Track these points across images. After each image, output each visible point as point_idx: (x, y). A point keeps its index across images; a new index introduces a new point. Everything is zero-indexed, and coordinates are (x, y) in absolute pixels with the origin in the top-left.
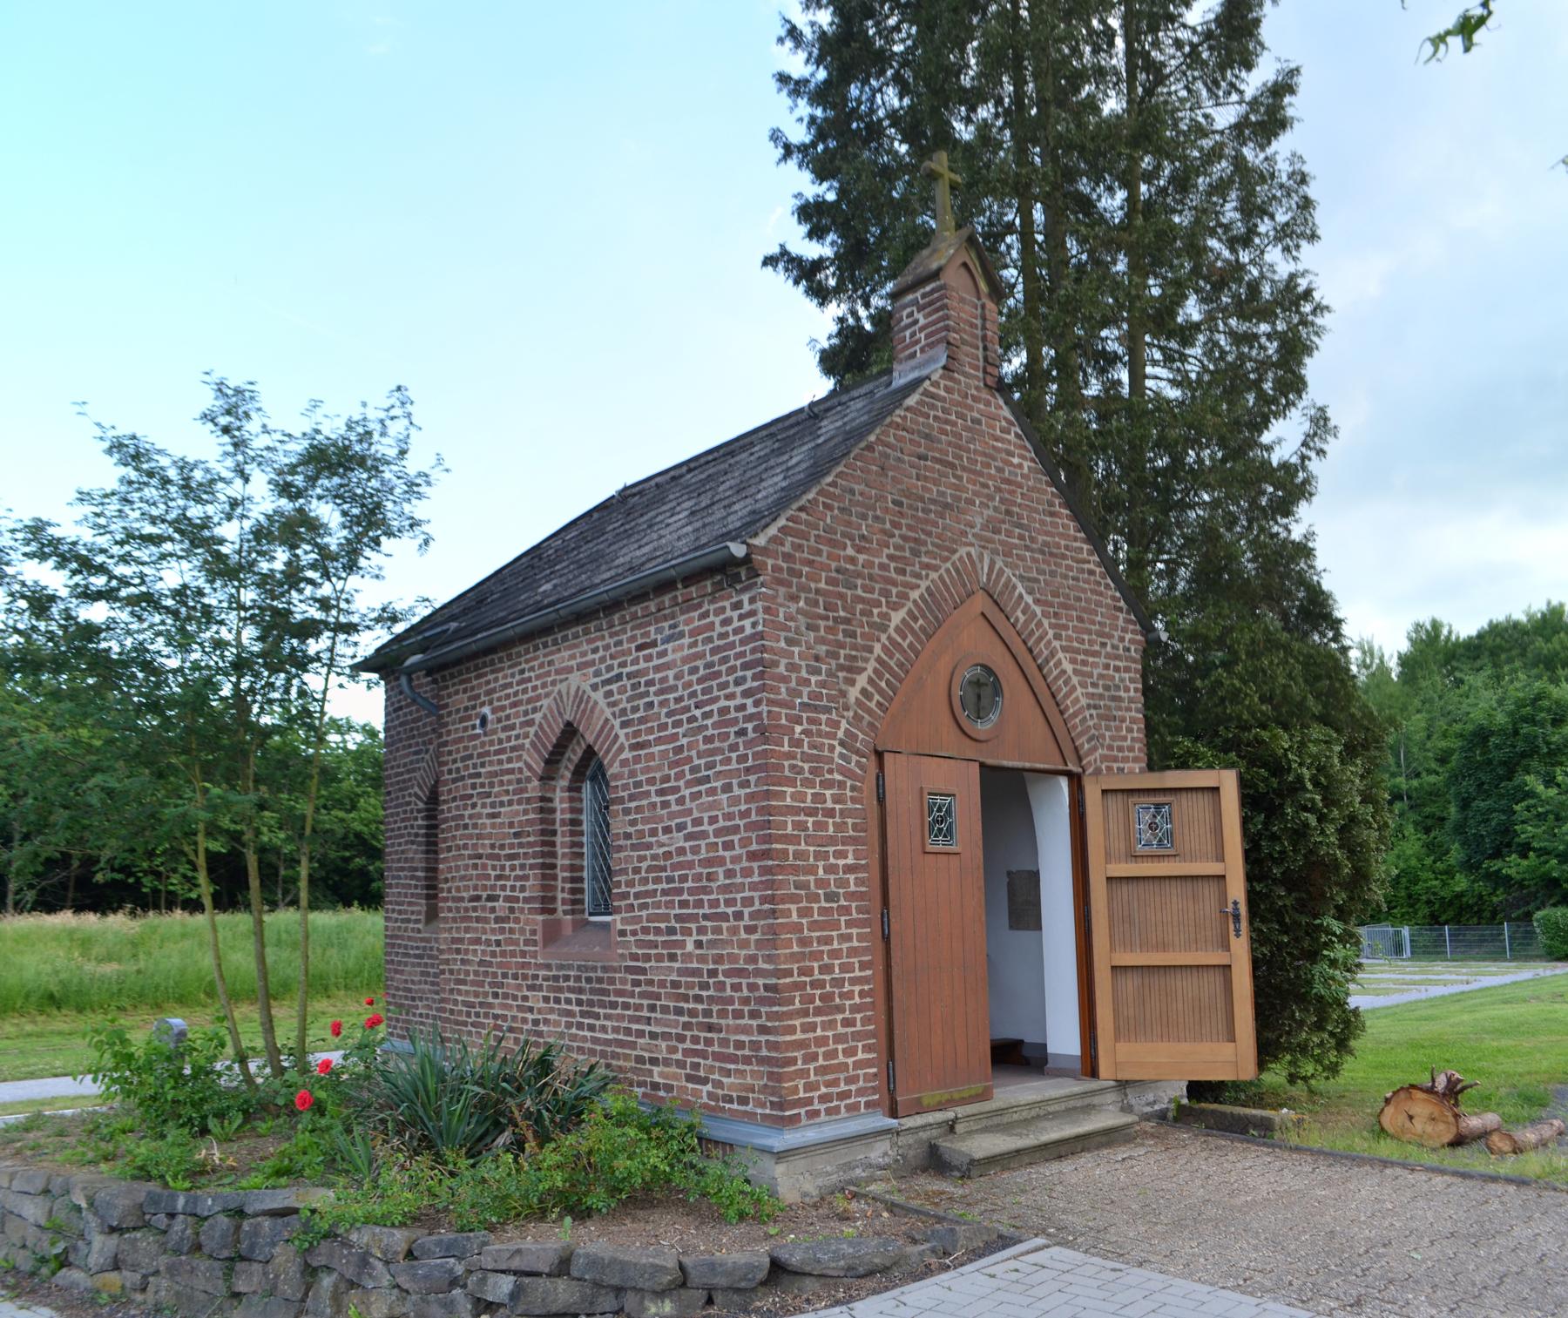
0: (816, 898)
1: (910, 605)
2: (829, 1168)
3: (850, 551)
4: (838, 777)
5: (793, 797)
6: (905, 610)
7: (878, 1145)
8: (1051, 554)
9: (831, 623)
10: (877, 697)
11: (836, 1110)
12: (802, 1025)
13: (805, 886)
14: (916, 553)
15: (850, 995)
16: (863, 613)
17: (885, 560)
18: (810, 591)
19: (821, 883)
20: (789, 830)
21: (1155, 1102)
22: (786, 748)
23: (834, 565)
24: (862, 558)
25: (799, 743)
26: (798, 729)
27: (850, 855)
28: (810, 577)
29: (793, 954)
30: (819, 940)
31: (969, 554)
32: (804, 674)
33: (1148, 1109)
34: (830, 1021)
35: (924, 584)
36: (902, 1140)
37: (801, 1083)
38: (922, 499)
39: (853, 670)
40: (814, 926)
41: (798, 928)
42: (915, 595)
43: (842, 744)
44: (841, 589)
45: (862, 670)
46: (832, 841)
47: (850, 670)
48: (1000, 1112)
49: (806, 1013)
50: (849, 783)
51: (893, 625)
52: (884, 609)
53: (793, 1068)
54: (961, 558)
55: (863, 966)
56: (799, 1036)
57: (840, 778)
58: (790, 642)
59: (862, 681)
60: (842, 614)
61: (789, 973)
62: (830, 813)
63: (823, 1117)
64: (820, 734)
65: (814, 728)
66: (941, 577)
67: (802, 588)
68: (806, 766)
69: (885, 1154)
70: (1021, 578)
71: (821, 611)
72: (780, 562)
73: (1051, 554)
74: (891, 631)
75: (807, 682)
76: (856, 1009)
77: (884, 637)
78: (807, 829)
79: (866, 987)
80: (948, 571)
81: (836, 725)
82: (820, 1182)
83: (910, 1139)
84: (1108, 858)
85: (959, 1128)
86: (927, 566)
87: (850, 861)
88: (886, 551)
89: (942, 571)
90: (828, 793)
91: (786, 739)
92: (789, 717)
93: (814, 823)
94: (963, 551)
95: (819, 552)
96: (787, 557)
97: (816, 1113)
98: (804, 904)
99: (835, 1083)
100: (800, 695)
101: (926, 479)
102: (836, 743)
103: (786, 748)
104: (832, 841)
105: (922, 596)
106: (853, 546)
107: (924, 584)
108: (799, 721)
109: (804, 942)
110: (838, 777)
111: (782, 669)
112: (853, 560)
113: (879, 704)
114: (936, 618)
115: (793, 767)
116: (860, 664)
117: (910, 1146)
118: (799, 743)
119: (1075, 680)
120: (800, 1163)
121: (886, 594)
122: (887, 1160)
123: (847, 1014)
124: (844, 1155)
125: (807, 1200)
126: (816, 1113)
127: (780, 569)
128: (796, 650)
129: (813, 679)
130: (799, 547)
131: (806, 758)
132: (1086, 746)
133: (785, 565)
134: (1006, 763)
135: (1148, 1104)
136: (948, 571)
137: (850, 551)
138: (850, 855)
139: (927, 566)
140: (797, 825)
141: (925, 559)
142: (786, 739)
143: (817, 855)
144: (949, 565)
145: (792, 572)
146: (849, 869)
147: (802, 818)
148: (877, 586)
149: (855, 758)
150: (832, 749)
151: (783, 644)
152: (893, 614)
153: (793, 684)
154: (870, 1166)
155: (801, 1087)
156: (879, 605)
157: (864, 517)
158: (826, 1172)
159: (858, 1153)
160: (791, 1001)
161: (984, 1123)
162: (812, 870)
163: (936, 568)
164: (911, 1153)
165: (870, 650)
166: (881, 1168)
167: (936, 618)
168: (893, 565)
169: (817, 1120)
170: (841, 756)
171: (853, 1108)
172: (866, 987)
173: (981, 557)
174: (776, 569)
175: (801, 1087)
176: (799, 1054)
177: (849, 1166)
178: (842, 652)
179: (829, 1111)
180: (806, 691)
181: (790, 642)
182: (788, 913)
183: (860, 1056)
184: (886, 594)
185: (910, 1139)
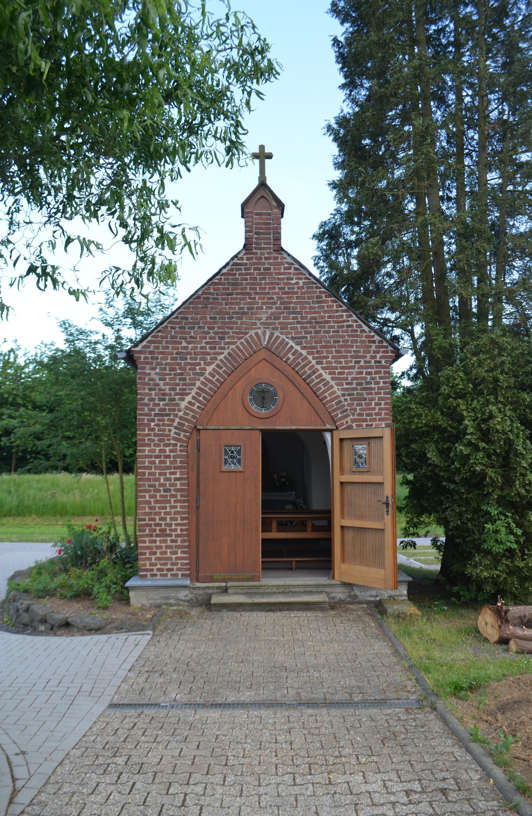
0: (159, 491)
1: (218, 362)
2: (156, 597)
3: (184, 344)
4: (172, 442)
5: (149, 451)
6: (215, 364)
7: (182, 592)
8: (317, 323)
9: (172, 376)
10: (197, 404)
11: (166, 575)
12: (149, 540)
13: (154, 486)
14: (223, 338)
15: (175, 530)
16: (190, 369)
17: (204, 345)
18: (162, 364)
19: (161, 485)
20: (147, 464)
21: (377, 596)
22: (147, 432)
23: (175, 352)
24: (190, 346)
25: (153, 429)
26: (153, 424)
27: (178, 474)
28: (162, 359)
29: (145, 513)
30: (159, 508)
31: (256, 334)
32: (157, 402)
33: (372, 599)
34: (164, 540)
35: (226, 352)
36: (196, 592)
37: (148, 563)
38: (228, 313)
39: (183, 394)
40: (156, 502)
41: (149, 503)
42: (222, 357)
43: (176, 428)
44: (179, 361)
45: (188, 394)
46: (169, 468)
47: (181, 394)
48: (258, 587)
49: (151, 536)
50: (179, 444)
51: (207, 372)
52: (202, 366)
53: (144, 557)
54: (251, 336)
55: (182, 519)
56: (147, 544)
57: (174, 442)
58: (150, 390)
59: (188, 398)
60: (179, 371)
61: (144, 520)
62: (168, 457)
63: (158, 577)
64: (164, 425)
65: (161, 423)
66: (237, 347)
67: (158, 364)
68: (156, 439)
69: (186, 596)
70: (293, 338)
71: (168, 372)
72: (148, 355)
73: (317, 323)
74: (207, 375)
75: (158, 405)
76: (177, 536)
77: (202, 378)
78: (155, 463)
79: (184, 528)
80: (242, 343)
81: (173, 421)
82: (151, 601)
83: (201, 592)
84: (342, 471)
85: (230, 591)
86: (229, 343)
87: (178, 476)
88: (204, 341)
89: (238, 344)
90: (167, 449)
91: (147, 429)
92: (148, 420)
93: (159, 461)
94: (252, 332)
95: (167, 348)
96: (151, 353)
97: (156, 575)
98: (152, 493)
99: (166, 564)
100: (154, 410)
101: (231, 303)
102: (172, 428)
103: (147, 432)
104: (169, 468)
105: (225, 357)
106: (186, 342)
107: (226, 352)
108: (153, 421)
109: (151, 508)
110: (172, 442)
111: (146, 401)
112: (185, 348)
113: (198, 407)
114: (233, 366)
115: (149, 439)
116: (188, 391)
117: (200, 595)
118: (153, 429)
119: (332, 383)
120: (142, 593)
121: (204, 359)
122: (186, 598)
123: (173, 538)
124: (164, 593)
125: (144, 607)
126: (156, 575)
127: (148, 358)
128: (153, 392)
129: (161, 403)
130: (157, 348)
131: (156, 435)
132: (340, 415)
133: (150, 356)
134: (278, 428)
135: (372, 596)
136: (242, 343)
137: (184, 344)
138: (178, 474)
139: (229, 343)
140: (150, 462)
141: (227, 340)
142: (147, 429)
143: (160, 474)
144: (242, 340)
145: (153, 358)
146: (176, 479)
147: (153, 459)
148: (199, 357)
149: (182, 433)
150: (170, 431)
151: (147, 391)
152: (207, 367)
153: (151, 406)
154: (178, 599)
155: (148, 564)
156: (199, 364)
157: (193, 328)
158: (156, 597)
159: (172, 593)
160: (145, 531)
161: (246, 591)
162: (158, 480)
163: (234, 343)
164: (200, 598)
165: (194, 385)
166: (184, 601)
167: (233, 366)
168: (208, 346)
169: (155, 578)
170: (175, 433)
171: (176, 575)
172: (184, 528)
173: (264, 333)
174: (145, 358)
175: (148, 564)
176: (147, 552)
177: (167, 598)
178: (178, 387)
179: (161, 575)
180: (157, 408)
181: (150, 390)
182: (144, 497)
183: (179, 555)
184: (204, 359)
185: (201, 592)
